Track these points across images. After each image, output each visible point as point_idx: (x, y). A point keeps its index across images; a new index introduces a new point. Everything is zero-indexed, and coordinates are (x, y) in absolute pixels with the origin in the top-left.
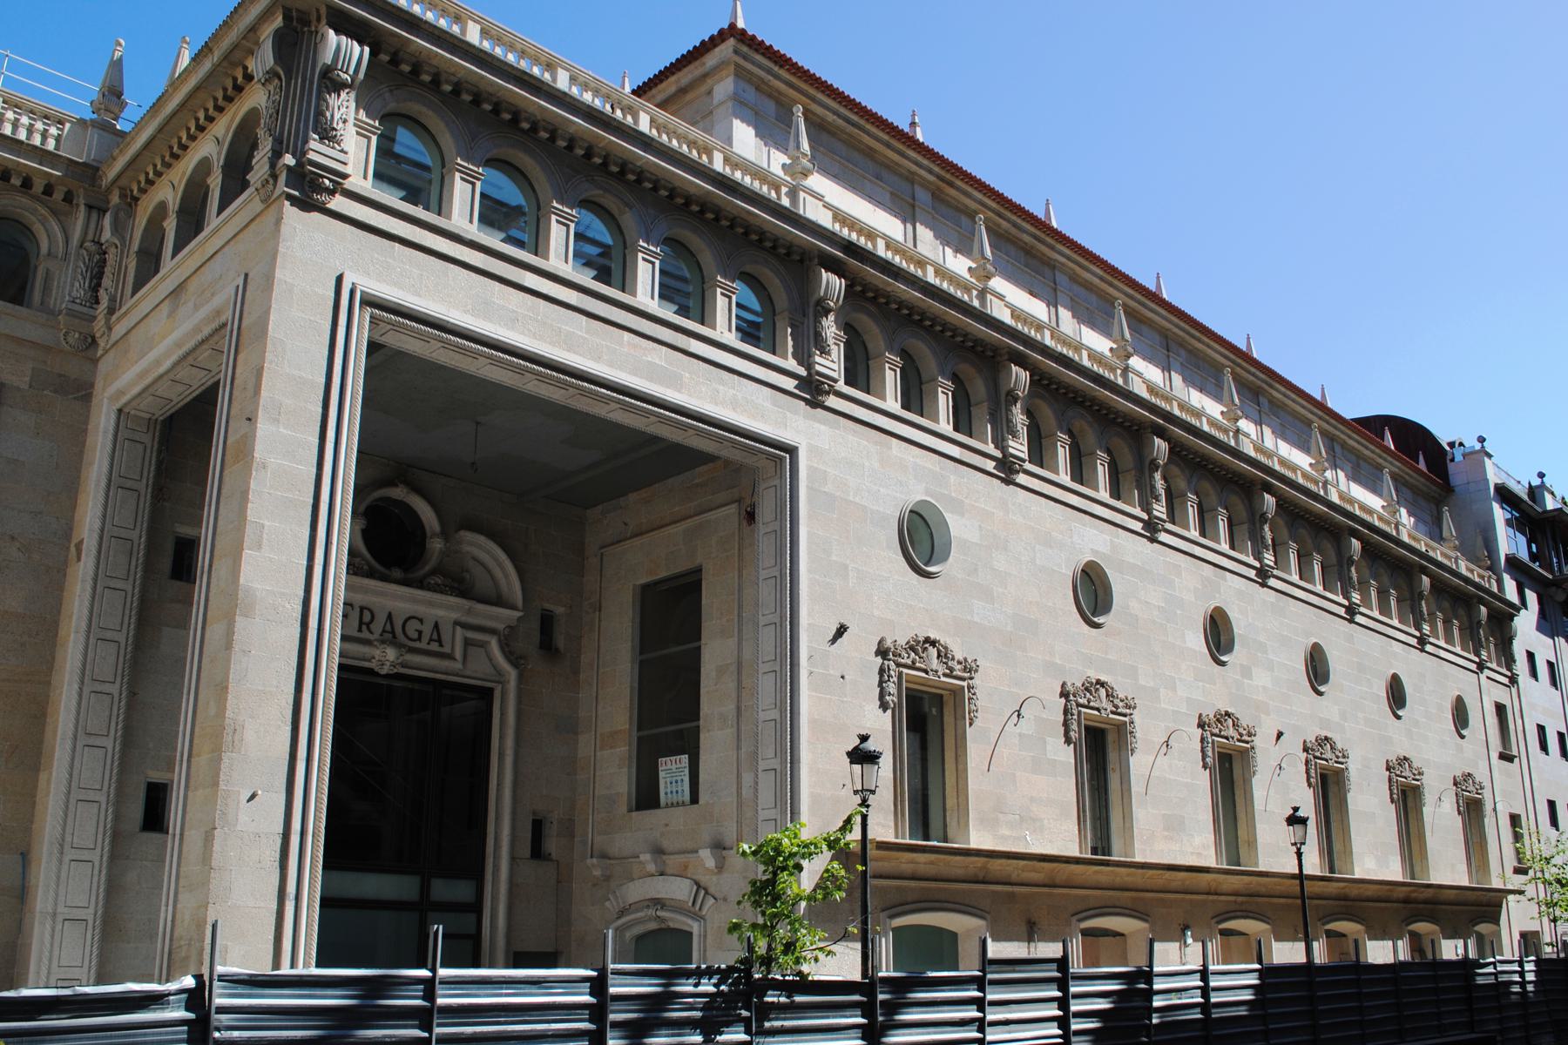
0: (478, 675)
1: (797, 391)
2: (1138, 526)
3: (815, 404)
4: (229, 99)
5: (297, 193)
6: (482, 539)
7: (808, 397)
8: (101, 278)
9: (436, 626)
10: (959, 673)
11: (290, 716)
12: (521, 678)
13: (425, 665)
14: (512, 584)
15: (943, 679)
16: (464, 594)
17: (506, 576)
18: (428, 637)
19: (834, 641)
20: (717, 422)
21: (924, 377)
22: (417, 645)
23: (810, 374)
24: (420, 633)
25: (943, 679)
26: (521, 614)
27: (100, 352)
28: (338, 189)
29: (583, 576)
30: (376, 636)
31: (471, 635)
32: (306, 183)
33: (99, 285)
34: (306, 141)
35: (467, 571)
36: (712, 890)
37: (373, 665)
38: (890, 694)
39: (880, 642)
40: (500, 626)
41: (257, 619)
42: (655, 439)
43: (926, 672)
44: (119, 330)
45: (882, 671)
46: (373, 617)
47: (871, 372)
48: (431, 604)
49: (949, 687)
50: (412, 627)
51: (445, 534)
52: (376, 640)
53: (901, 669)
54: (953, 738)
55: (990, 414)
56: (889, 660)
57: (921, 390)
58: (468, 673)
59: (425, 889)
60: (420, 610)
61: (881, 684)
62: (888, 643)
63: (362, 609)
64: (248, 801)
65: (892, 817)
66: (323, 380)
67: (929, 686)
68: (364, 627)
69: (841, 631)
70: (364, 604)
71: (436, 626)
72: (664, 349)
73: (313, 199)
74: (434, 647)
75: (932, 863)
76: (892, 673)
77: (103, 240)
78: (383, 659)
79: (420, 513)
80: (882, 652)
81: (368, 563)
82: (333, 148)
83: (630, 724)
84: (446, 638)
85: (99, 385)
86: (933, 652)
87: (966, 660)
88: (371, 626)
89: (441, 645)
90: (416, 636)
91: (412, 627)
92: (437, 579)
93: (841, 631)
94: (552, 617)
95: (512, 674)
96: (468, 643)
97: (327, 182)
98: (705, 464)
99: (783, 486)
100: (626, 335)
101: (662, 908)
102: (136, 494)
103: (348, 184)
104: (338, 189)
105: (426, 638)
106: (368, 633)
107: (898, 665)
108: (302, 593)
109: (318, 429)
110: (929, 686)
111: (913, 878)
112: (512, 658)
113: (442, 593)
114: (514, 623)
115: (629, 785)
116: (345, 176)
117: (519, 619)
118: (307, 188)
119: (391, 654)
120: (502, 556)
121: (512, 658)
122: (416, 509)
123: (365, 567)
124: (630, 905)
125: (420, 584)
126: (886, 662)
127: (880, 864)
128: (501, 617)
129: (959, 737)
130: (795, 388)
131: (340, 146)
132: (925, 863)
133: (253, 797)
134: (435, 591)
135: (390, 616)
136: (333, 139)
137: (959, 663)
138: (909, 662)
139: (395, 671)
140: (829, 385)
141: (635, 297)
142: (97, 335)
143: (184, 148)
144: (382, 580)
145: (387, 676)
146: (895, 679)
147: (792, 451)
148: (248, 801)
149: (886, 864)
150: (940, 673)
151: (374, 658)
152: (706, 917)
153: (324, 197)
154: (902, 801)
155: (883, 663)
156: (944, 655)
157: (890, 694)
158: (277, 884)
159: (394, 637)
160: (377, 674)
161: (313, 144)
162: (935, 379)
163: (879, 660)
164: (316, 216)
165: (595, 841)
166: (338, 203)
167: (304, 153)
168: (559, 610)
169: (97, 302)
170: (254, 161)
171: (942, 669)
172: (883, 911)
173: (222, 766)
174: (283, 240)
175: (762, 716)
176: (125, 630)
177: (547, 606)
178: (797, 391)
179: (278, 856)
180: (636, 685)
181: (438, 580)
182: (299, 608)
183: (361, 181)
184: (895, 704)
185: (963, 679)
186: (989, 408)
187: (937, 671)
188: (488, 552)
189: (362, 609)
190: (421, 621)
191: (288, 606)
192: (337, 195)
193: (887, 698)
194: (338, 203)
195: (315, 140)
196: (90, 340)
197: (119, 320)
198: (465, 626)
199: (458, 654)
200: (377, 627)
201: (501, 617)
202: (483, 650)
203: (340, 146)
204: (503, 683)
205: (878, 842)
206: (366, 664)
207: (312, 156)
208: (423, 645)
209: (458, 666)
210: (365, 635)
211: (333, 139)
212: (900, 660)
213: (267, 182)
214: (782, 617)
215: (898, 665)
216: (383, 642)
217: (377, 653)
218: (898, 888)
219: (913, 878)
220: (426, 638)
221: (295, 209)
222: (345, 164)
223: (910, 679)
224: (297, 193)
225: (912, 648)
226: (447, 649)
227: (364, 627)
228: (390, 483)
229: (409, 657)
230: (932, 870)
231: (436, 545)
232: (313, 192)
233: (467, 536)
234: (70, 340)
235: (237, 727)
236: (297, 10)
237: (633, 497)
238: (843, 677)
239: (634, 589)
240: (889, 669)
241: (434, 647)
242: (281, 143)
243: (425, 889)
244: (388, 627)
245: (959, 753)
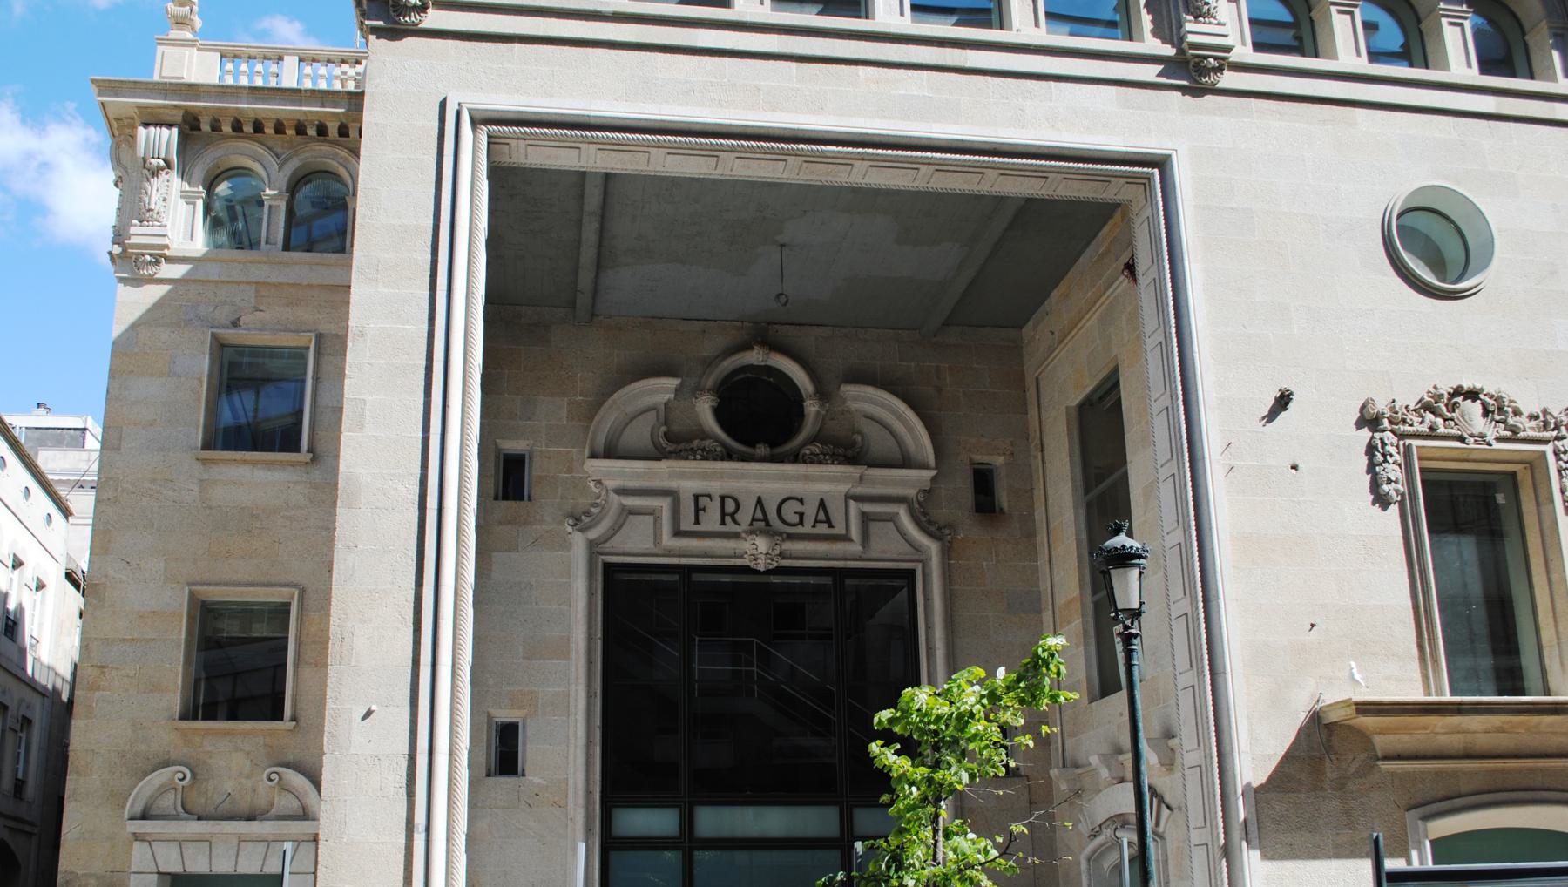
0: (888, 556)
1: (1163, 80)
2: (1150, 73)
3: (1197, 91)
5: (381, 23)
6: (870, 391)
7: (1185, 83)
9: (822, 503)
10: (1531, 433)
11: (412, 616)
12: (947, 552)
13: (809, 553)
14: (919, 439)
15: (1496, 446)
16: (852, 460)
17: (910, 429)
18: (814, 517)
19: (1272, 415)
20: (1024, 150)
21: (1422, 11)
22: (799, 530)
23: (1181, 51)
24: (801, 515)
25: (1496, 446)
26: (934, 472)
28: (1224, 65)
29: (1027, 414)
30: (745, 525)
31: (868, 508)
32: (1191, 67)
34: (1180, 26)
35: (859, 433)
36: (1167, 798)
37: (746, 562)
38: (1389, 481)
39: (1363, 407)
40: (911, 492)
41: (363, 509)
42: (1000, 201)
43: (1461, 439)
45: (1371, 449)
46: (738, 506)
47: (1317, 27)
48: (806, 478)
49: (1518, 457)
50: (790, 512)
51: (823, 394)
52: (745, 532)
53: (1408, 442)
54: (1538, 535)
55: (1555, 35)
56: (1383, 431)
57: (1421, 32)
58: (874, 555)
59: (687, 822)
60: (797, 488)
61: (1371, 468)
62: (1381, 405)
63: (723, 498)
64: (363, 719)
65: (1415, 666)
66: (430, 222)
67: (1475, 461)
68: (728, 519)
69: (1283, 401)
70: (723, 492)
71: (822, 503)
72: (925, 74)
73: (1202, 84)
74: (822, 529)
75: (1500, 730)
76: (1389, 448)
78: (755, 552)
79: (790, 375)
80: (1368, 421)
81: (723, 444)
82: (1210, 23)
83: (1081, 588)
86: (1475, 408)
87: (1545, 412)
88: (737, 516)
89: (831, 526)
90: (796, 519)
91: (790, 512)
92: (813, 448)
93: (1283, 401)
94: (991, 471)
95: (933, 548)
96: (866, 518)
97: (1212, 60)
98: (1105, 223)
99: (1155, 214)
100: (861, 69)
101: (1122, 826)
103: (1234, 57)
104: (1224, 65)
105: (809, 520)
106: (733, 524)
107: (1401, 436)
108: (418, 471)
109: (427, 279)
110: (1475, 461)
111: (1468, 755)
112: (932, 529)
113: (820, 463)
114: (927, 486)
115: (1088, 667)
116: (1228, 49)
117: (934, 479)
118: (1194, 74)
119: (762, 544)
120: (902, 407)
121: (932, 529)
122: (787, 372)
123: (719, 449)
124: (1100, 826)
125: (795, 458)
126: (1377, 435)
127: (1391, 737)
128: (911, 481)
129: (1547, 532)
130: (1158, 75)
131: (1215, 18)
132: (1487, 732)
133: (369, 713)
134: (812, 462)
135: (759, 501)
136: (1209, 14)
137: (1533, 417)
138: (1424, 429)
139: (775, 565)
140: (1216, 58)
141: (1449, 70)
144: (743, 460)
145: (768, 572)
146: (1400, 459)
147: (1161, 163)
148: (363, 719)
149: (1405, 738)
150: (1490, 437)
151: (746, 553)
152: (1166, 835)
153: (413, 18)
154: (1432, 639)
155: (1373, 437)
156: (1495, 409)
157: (1389, 481)
158: (405, 814)
159: (768, 524)
160: (756, 572)
161: (1189, 26)
162: (1434, 9)
163: (1365, 434)
164: (410, 42)
165: (1067, 747)
166: (1228, 80)
167: (1182, 39)
168: (999, 461)
171: (1491, 432)
172: (1409, 809)
173: (329, 681)
174: (370, 79)
177: (978, 458)
178: (1163, 80)
179: (404, 781)
180: (1084, 536)
181: (816, 448)
182: (416, 489)
183: (1244, 52)
184: (1403, 495)
185: (1545, 442)
186: (1550, 28)
187: (1482, 436)
188: (882, 406)
189: (723, 498)
190: (801, 501)
191: (401, 488)
192: (1225, 72)
193: (1385, 487)
194: (1228, 80)
195: (1190, 21)
198: (859, 499)
199: (855, 532)
200: (745, 516)
201: (911, 481)
202: (891, 524)
203: (1215, 18)
204: (925, 563)
205: (1357, 704)
206: (738, 562)
207: (1191, 38)
208: (807, 529)
209: (855, 548)
210: (730, 527)
211: (1209, 14)
212: (1403, 428)
214: (1173, 397)
215: (1401, 436)
216: (752, 532)
217: (745, 545)
218: (1438, 773)
219: (1468, 755)
220: (809, 520)
221: (383, 41)
222: (1226, 36)
223: (1426, 453)
224: (381, 23)
225: (1428, 408)
226: (839, 529)
227: (728, 519)
228: (747, 347)
229: (788, 546)
230: (1504, 742)
231: (811, 408)
232: (399, 15)
233: (849, 390)
235: (346, 635)
237: (1055, 294)
238: (1294, 467)
239: (1068, 414)
240: (1383, 444)
241: (822, 529)
243: (687, 822)
244: (759, 515)
245: (1550, 556)
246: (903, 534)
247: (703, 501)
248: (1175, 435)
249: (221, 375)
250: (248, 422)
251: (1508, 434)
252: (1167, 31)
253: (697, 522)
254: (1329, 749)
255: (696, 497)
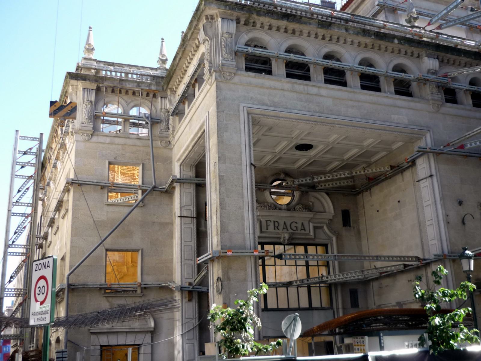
4: (196, 51)
8: (169, 121)
12: (337, 238)
22: (296, 232)
24: (297, 227)
27: (172, 146)
33: (168, 123)
44: (176, 138)
50: (294, 225)
63: (274, 222)
68: (276, 228)
77: (167, 108)
84: (307, 228)
85: (173, 158)
89: (305, 231)
90: (295, 229)
91: (294, 225)
96: (315, 228)
102: (190, 193)
135: (285, 223)
142: (171, 140)
143: (186, 71)
169: (169, 129)
170: (205, 71)
175: (431, 243)
176: (193, 241)
189: (274, 222)
190: (296, 223)
196: (168, 143)
197: (176, 134)
200: (281, 227)
208: (299, 232)
213: (209, 78)
226: (307, 232)
227: (276, 228)
234: (162, 144)
236: (210, 15)
241: (303, 231)
242: (212, 63)
246: (325, 233)
247: (269, 222)
248: (397, 170)
249: (217, 230)
250: (22, 254)
251: (10, 242)
252: (199, 71)
253: (267, 229)
254: (154, 188)
255: (267, 221)
